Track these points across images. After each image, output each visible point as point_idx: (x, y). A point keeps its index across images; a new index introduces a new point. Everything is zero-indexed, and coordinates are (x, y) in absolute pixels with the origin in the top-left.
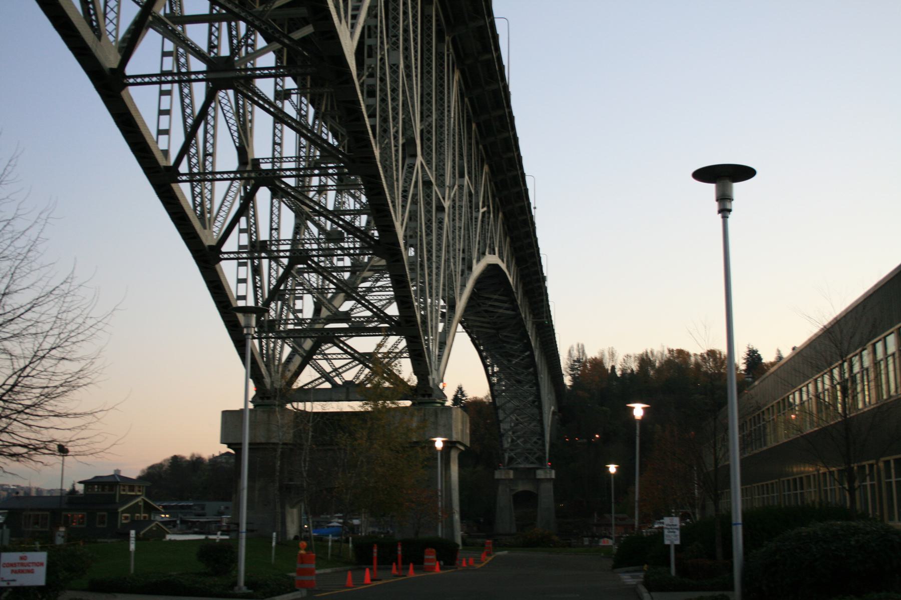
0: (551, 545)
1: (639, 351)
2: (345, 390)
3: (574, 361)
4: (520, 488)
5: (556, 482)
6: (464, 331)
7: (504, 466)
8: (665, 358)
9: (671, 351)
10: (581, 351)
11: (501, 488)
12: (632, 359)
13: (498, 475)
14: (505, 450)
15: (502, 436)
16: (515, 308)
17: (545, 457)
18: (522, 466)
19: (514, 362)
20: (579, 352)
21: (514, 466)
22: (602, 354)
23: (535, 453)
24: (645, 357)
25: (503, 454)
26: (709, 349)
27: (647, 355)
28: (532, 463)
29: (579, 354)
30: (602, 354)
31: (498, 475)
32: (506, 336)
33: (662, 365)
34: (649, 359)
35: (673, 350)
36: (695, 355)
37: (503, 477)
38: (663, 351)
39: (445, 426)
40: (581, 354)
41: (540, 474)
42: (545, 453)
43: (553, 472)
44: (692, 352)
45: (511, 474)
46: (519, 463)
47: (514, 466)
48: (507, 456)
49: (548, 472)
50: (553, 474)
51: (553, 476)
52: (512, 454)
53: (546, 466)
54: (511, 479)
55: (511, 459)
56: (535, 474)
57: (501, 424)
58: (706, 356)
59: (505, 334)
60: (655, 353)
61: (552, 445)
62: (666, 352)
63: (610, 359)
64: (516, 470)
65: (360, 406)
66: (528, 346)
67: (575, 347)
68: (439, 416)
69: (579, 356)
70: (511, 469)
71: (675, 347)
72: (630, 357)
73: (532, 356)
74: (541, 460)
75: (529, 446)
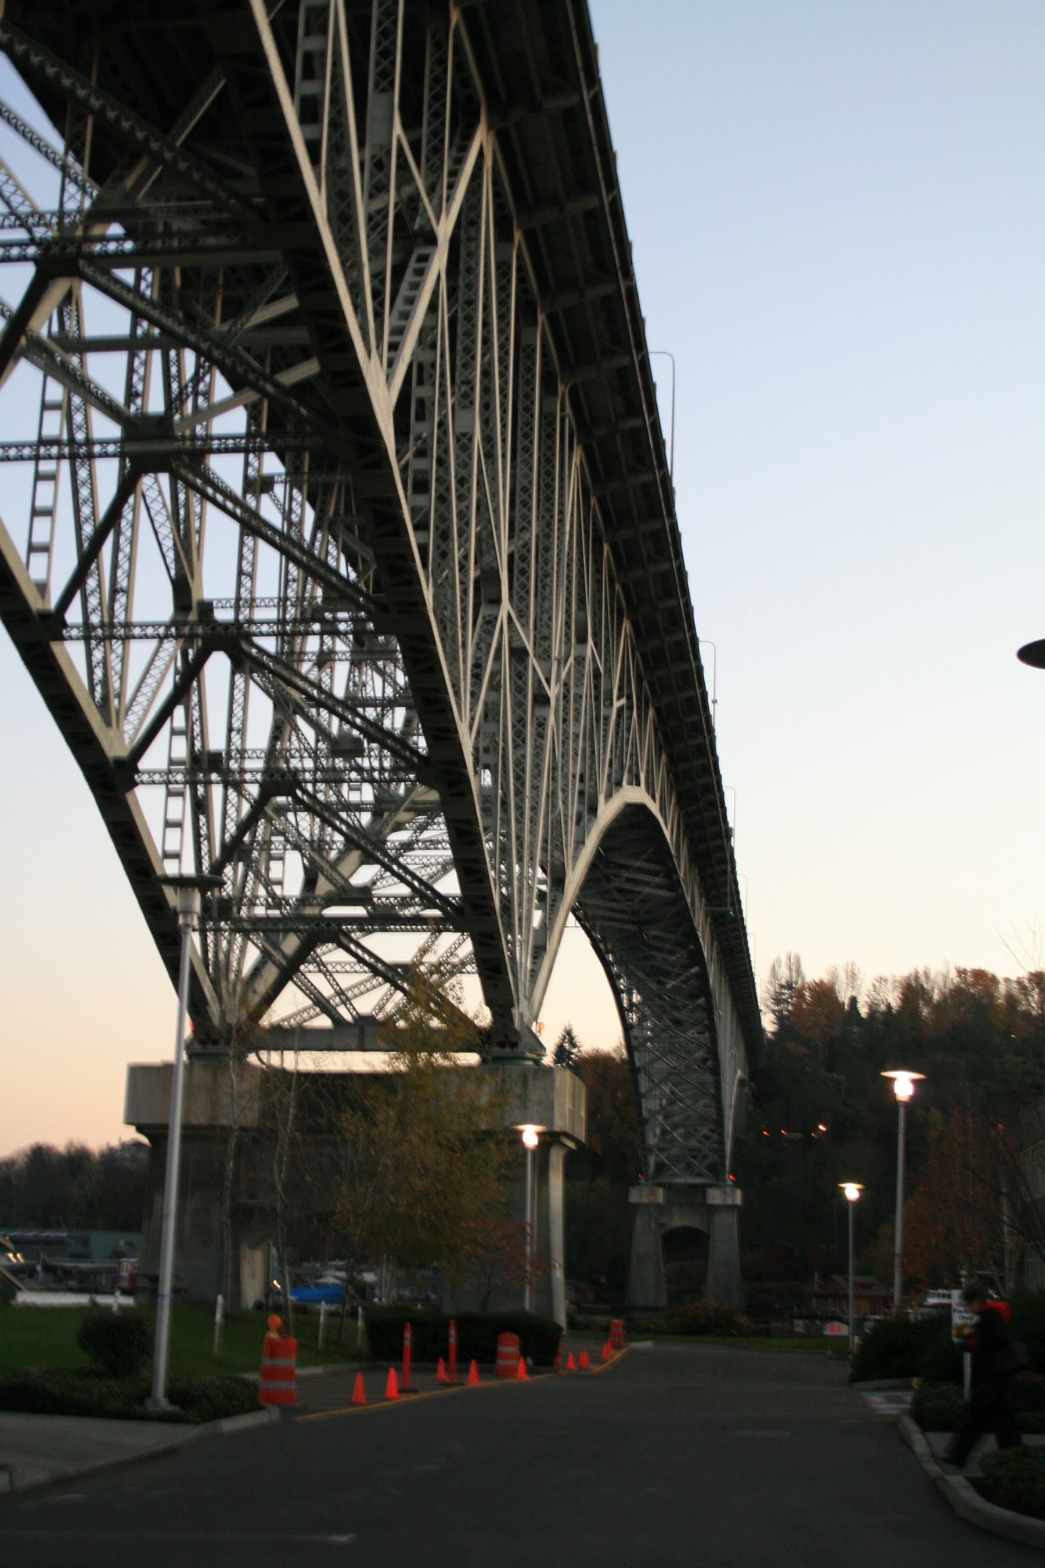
0: (734, 1332)
1: (902, 969)
2: (357, 1031)
3: (782, 986)
4: (678, 1221)
5: (743, 1213)
6: (578, 925)
7: (647, 1180)
8: (950, 985)
9: (961, 973)
10: (793, 968)
11: (640, 1221)
12: (890, 986)
13: (635, 1196)
14: (649, 1150)
15: (643, 1122)
16: (674, 885)
17: (724, 1165)
18: (680, 1180)
19: (669, 986)
20: (790, 970)
21: (665, 1179)
22: (835, 976)
23: (704, 1157)
24: (913, 983)
25: (646, 1157)
26: (1033, 971)
27: (917, 978)
28: (700, 1175)
29: (791, 975)
30: (835, 976)
31: (635, 1196)
32: (654, 937)
33: (944, 998)
34: (922, 986)
35: (965, 972)
36: (1007, 980)
37: (645, 1200)
38: (948, 972)
39: (540, 1102)
40: (794, 973)
41: (715, 1197)
42: (723, 1158)
43: (739, 1193)
44: (1000, 975)
45: (660, 1195)
46: (675, 1175)
47: (665, 1179)
48: (652, 1160)
49: (729, 1192)
50: (738, 1197)
51: (739, 1201)
52: (663, 1158)
53: (724, 1181)
54: (658, 1206)
55: (660, 1167)
56: (704, 1196)
57: (643, 1101)
58: (1026, 983)
59: (654, 933)
60: (932, 975)
61: (737, 1142)
62: (953, 975)
63: (847, 984)
64: (669, 1187)
65: (385, 1062)
66: (697, 957)
67: (784, 960)
68: (530, 1082)
69: (791, 975)
70: (660, 1185)
71: (971, 964)
72: (886, 981)
73: (703, 976)
74: (716, 1170)
75: (693, 1143)
